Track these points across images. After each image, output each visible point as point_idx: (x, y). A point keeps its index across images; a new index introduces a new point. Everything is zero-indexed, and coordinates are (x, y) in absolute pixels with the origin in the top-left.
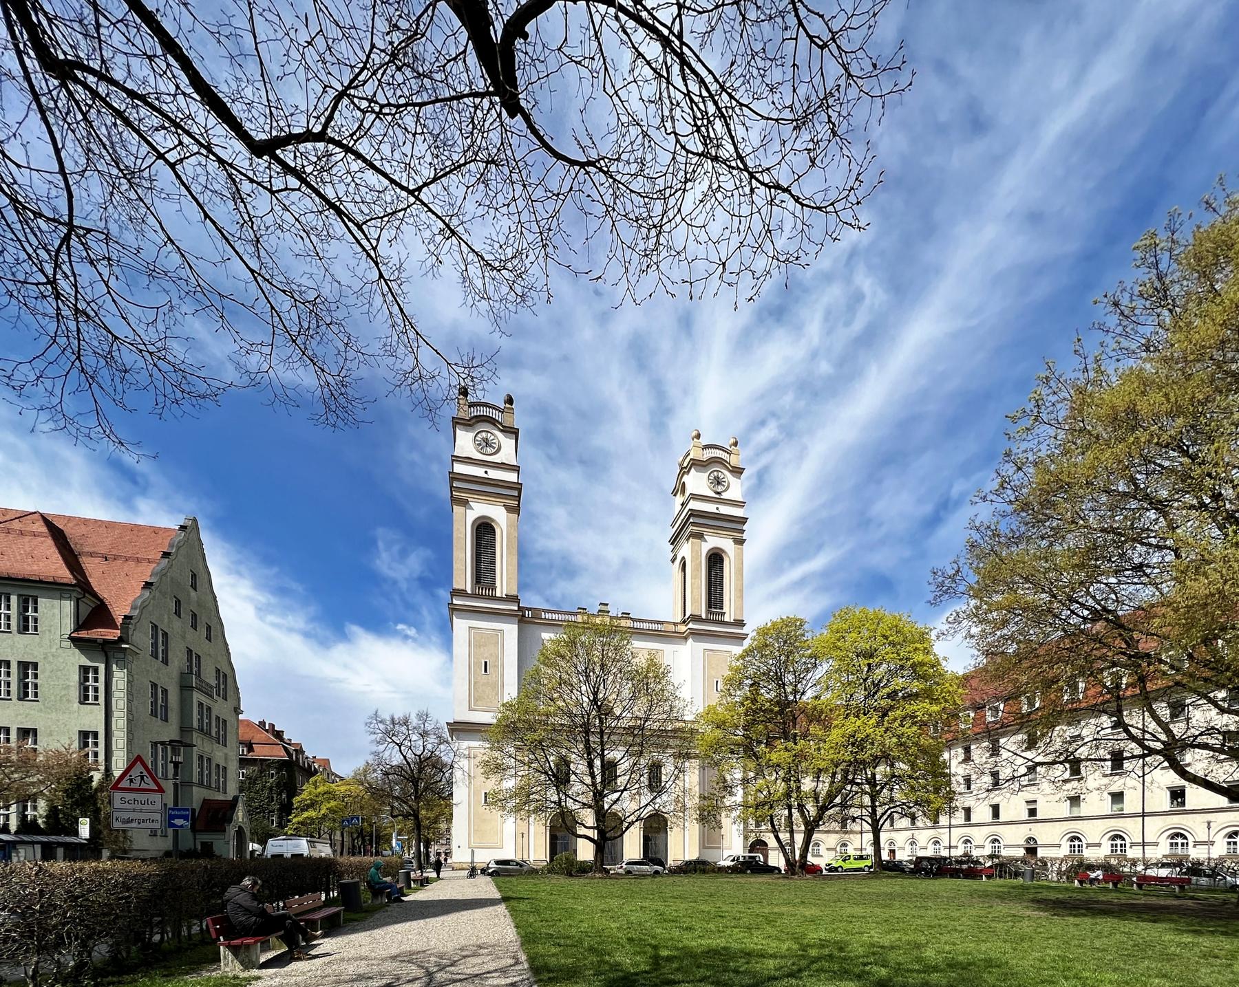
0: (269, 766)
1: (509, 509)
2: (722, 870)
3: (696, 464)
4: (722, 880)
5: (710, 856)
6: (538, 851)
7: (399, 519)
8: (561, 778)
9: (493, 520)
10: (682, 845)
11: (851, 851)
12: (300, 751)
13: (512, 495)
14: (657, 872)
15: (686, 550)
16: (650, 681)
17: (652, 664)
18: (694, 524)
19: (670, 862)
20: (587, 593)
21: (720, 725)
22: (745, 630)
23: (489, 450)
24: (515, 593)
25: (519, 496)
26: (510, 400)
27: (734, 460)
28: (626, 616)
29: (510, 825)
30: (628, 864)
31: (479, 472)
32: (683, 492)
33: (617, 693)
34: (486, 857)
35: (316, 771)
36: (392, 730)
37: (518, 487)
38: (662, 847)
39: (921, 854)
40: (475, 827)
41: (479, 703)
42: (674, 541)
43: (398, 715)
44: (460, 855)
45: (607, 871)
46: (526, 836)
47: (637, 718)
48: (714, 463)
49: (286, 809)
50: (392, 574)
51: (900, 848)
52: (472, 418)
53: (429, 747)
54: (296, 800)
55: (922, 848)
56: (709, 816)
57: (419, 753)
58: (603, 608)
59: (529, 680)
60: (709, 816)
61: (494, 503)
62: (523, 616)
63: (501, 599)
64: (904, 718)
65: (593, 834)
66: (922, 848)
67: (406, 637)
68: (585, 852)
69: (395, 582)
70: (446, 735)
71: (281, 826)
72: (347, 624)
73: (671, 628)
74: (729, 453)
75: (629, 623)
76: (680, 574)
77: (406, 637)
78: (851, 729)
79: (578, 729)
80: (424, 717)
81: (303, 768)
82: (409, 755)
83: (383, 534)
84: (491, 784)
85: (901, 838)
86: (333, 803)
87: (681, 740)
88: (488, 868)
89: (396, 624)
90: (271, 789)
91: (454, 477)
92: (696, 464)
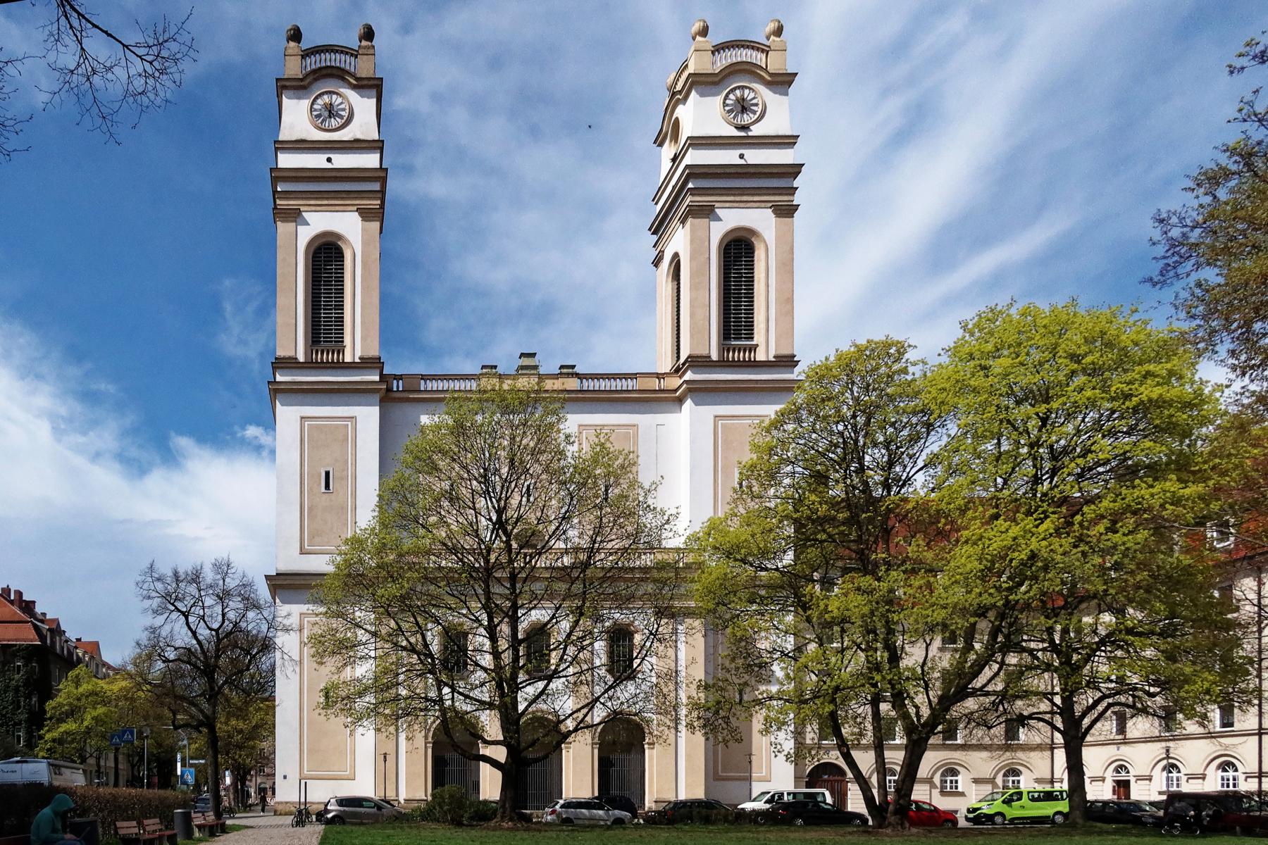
0: (14, 655)
1: (366, 214)
2: (754, 817)
5: (726, 794)
6: (412, 784)
8: (455, 658)
9: (339, 237)
10: (674, 770)
11: (1026, 783)
12: (57, 631)
13: (369, 192)
14: (619, 822)
15: (680, 240)
16: (606, 487)
17: (602, 452)
18: (694, 191)
19: (649, 803)
22: (797, 374)
23: (334, 123)
24: (374, 352)
26: (368, 34)
27: (774, 64)
28: (568, 371)
29: (366, 739)
30: (568, 805)
31: (315, 161)
32: (675, 138)
33: (538, 505)
34: (323, 793)
35: (79, 661)
36: (176, 592)
37: (380, 175)
39: (1188, 787)
40: (311, 748)
41: (317, 540)
42: (659, 227)
43: (185, 567)
44: (286, 793)
45: (528, 819)
46: (391, 759)
47: (577, 549)
49: (37, 719)
51: (1139, 778)
52: (307, 75)
53: (232, 615)
54: (50, 705)
55: (1191, 777)
56: (722, 721)
57: (215, 626)
58: (527, 362)
59: (396, 498)
60: (722, 721)
61: (343, 209)
62: (389, 390)
63: (352, 367)
65: (500, 754)
66: (1191, 777)
68: (490, 785)
70: (263, 592)
71: (31, 745)
73: (654, 384)
74: (765, 50)
75: (573, 384)
78: (996, 546)
79: (489, 576)
81: (61, 657)
82: (203, 632)
84: (327, 673)
85: (1142, 758)
86: (101, 710)
87: (664, 587)
88: (327, 811)
89: (244, 429)
90: (17, 689)
91: (279, 175)
92: (704, 83)
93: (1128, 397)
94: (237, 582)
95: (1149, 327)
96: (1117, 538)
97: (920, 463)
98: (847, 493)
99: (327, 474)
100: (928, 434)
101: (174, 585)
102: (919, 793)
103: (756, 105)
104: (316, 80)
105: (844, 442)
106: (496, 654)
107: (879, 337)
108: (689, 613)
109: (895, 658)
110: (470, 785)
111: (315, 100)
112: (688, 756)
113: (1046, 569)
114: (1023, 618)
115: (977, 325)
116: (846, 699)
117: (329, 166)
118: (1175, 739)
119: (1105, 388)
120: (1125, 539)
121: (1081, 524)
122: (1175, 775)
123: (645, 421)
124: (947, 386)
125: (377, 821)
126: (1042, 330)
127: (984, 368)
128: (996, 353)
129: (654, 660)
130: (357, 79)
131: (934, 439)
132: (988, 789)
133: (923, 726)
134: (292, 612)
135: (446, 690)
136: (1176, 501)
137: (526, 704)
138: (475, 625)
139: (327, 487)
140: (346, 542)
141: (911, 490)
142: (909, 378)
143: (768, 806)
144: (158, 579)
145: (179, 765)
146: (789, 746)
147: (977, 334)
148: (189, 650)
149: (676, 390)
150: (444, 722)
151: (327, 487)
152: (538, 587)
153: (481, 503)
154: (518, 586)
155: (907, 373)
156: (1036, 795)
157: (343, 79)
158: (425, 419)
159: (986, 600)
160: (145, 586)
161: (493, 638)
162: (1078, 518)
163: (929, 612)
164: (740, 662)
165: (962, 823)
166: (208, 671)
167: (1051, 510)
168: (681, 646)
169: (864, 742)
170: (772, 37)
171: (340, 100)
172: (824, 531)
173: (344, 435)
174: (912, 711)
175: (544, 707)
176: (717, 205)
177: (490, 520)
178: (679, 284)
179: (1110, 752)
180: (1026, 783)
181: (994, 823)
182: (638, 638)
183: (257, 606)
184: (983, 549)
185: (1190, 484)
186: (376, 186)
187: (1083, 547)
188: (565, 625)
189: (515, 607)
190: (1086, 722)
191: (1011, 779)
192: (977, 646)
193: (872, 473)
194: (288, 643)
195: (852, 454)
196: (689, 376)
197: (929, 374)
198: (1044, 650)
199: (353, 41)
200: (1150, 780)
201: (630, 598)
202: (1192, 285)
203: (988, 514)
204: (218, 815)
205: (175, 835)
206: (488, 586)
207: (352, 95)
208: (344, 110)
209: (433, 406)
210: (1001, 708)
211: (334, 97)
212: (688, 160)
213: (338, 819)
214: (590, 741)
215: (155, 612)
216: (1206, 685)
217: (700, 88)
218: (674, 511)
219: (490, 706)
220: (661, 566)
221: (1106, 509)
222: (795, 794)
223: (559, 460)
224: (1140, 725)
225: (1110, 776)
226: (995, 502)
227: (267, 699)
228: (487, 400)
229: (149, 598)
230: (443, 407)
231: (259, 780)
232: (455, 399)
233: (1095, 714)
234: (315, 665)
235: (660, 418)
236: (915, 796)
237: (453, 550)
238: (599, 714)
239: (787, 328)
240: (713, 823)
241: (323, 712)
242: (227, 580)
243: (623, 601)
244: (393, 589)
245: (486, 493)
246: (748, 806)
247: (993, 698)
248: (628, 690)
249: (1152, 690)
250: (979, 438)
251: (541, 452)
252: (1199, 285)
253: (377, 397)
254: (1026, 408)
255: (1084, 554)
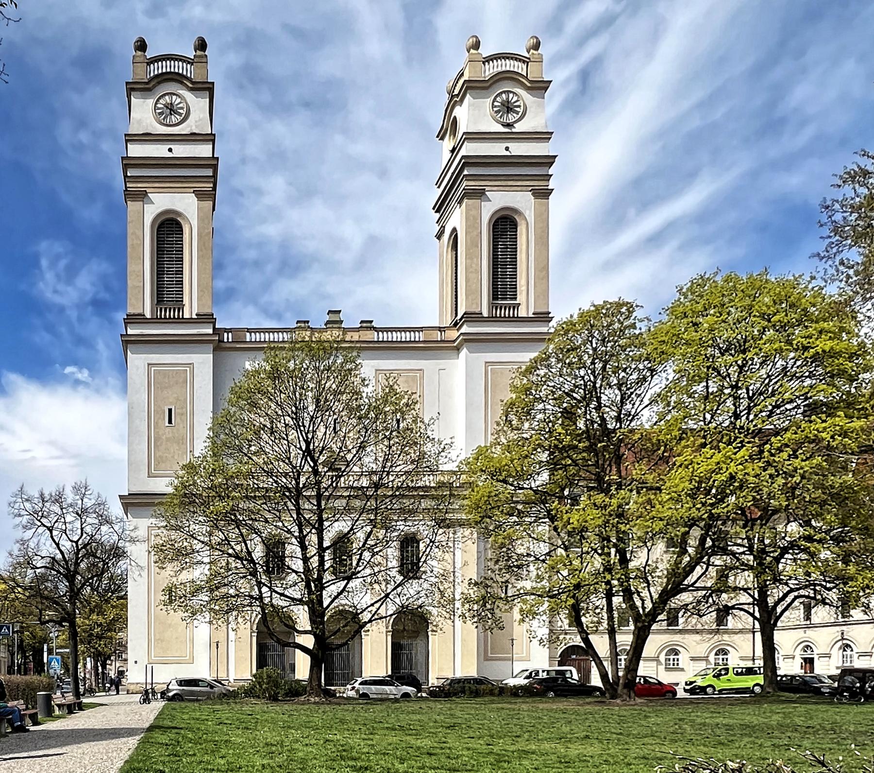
1: (200, 195)
2: (516, 692)
3: (475, 87)
4: (507, 705)
6: (240, 668)
7: (62, 224)
8: (276, 562)
9: (179, 214)
10: (452, 653)
13: (204, 178)
14: (406, 695)
15: (457, 218)
16: (394, 418)
20: (308, 298)
21: (496, 474)
23: (174, 119)
24: (207, 310)
25: (215, 176)
26: (202, 45)
28: (367, 325)
29: (202, 630)
31: (159, 151)
32: (454, 131)
34: (167, 676)
36: (42, 510)
37: (212, 163)
38: (421, 658)
39: (860, 664)
41: (163, 465)
42: (441, 206)
43: (49, 490)
44: (135, 676)
45: (332, 694)
48: (504, 81)
50: (58, 299)
51: (822, 656)
52: (152, 79)
53: (88, 529)
56: (488, 607)
57: (75, 539)
58: (334, 318)
60: (488, 607)
62: (221, 341)
63: (190, 321)
64: (800, 444)
65: (309, 641)
67: (77, 382)
69: (62, 309)
72: (5, 372)
73: (438, 336)
75: (374, 336)
76: (448, 256)
77: (77, 382)
80: (81, 490)
82: (66, 545)
83: (48, 249)
85: (823, 639)
89: (65, 365)
91: (128, 163)
92: (475, 87)
93: (806, 349)
94: (93, 501)
95: (824, 292)
96: (797, 462)
97: (646, 401)
98: (586, 426)
99: (170, 410)
100: (652, 376)
101: (40, 505)
102: (645, 669)
103: (519, 106)
104: (159, 83)
105: (585, 386)
106: (306, 560)
107: (613, 299)
108: (461, 524)
109: (624, 561)
110: (287, 667)
111: (158, 100)
112: (463, 640)
113: (741, 488)
114: (729, 528)
115: (690, 289)
116: (588, 594)
117: (170, 155)
118: (846, 624)
119: (789, 342)
120: (803, 463)
121: (769, 451)
122: (849, 652)
123: (428, 365)
124: (666, 339)
125: (209, 698)
126: (740, 294)
127: (695, 324)
128: (704, 312)
129: (434, 563)
130: (193, 83)
131: (657, 381)
132: (703, 665)
133: (646, 615)
134: (143, 526)
135: (264, 589)
136: (844, 434)
137: (330, 600)
138: (289, 536)
139: (170, 422)
140: (183, 467)
141: (639, 423)
142: (637, 332)
143: (527, 681)
144: (27, 500)
145: (45, 654)
146: (543, 632)
147: (690, 297)
148: (53, 558)
149: (454, 341)
150: (264, 615)
151: (170, 422)
152: (340, 504)
153: (293, 435)
154: (323, 503)
155: (635, 328)
156: (740, 670)
157: (182, 83)
158: (248, 365)
159: (694, 513)
160: (17, 506)
161: (304, 548)
162: (767, 447)
163: (649, 523)
164: (502, 564)
165: (681, 694)
166: (70, 577)
167: (746, 440)
168: (458, 553)
169: (601, 628)
170: (532, 51)
171: (179, 100)
172: (568, 457)
173: (182, 378)
174: (638, 603)
175: (343, 602)
176: (487, 188)
177: (301, 448)
178: (456, 254)
179: (799, 634)
180: (734, 661)
181: (706, 694)
182: (422, 546)
183: (108, 522)
184: (692, 472)
185: (855, 419)
186: (209, 172)
187: (771, 471)
188: (361, 535)
189: (321, 521)
190: (779, 609)
191: (721, 657)
192: (691, 550)
193: (607, 409)
194: (138, 553)
195: (592, 394)
196: (465, 329)
197: (652, 329)
198: (743, 553)
199: (191, 54)
200: (830, 657)
201: (412, 512)
202: (837, 263)
203: (698, 443)
204: (77, 695)
205: (36, 714)
206: (298, 504)
207: (188, 95)
208: (182, 108)
209: (252, 354)
210: (710, 600)
211: (174, 97)
212: (463, 152)
213: (177, 697)
214: (384, 630)
215: (25, 527)
216: (866, 582)
217: (474, 92)
218: (449, 441)
219: (300, 602)
220: (441, 485)
221: (789, 440)
222: (548, 671)
223: (356, 399)
224: (820, 614)
225: (798, 652)
226: (703, 432)
227: (122, 598)
228: (299, 349)
229: (20, 515)
230: (261, 355)
231: (118, 665)
232: (271, 349)
233: (784, 604)
234: (158, 570)
235: (442, 363)
236: (640, 672)
237: (270, 474)
238: (390, 608)
239: (543, 294)
240: (483, 696)
241: (164, 608)
242: (85, 500)
243: (408, 513)
244: (220, 505)
245: (297, 427)
246: (512, 682)
247: (704, 592)
248: (412, 588)
249: (828, 585)
250: (692, 381)
251: (342, 393)
252: (842, 263)
253: (211, 346)
254: (728, 358)
255: (771, 476)
